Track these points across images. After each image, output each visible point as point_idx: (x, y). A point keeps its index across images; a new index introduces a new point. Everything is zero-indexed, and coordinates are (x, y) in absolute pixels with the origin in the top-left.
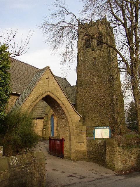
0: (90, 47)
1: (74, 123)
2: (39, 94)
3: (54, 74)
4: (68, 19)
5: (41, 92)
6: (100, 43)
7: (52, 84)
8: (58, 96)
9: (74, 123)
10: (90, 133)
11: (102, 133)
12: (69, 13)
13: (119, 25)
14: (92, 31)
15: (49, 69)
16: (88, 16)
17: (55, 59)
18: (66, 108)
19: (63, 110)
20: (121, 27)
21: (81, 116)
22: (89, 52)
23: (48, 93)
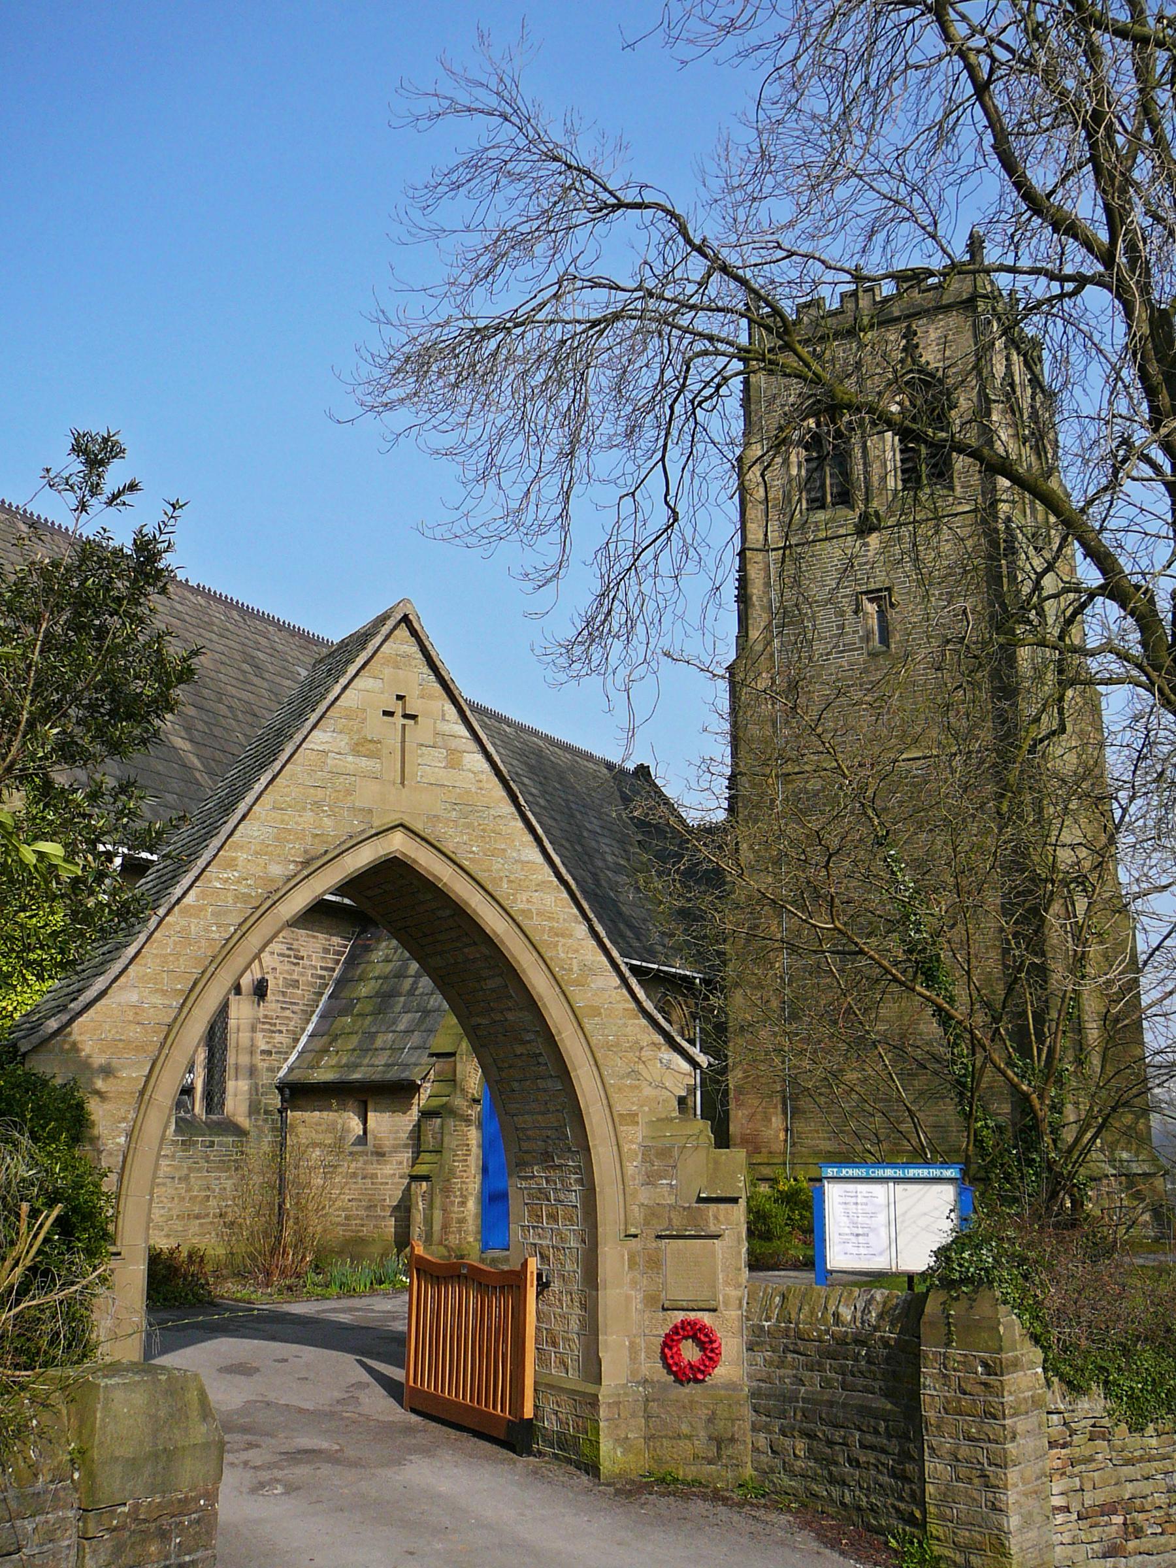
0: (844, 498)
1: (632, 1118)
2: (295, 850)
3: (467, 690)
4: (622, 251)
5: (332, 828)
6: (927, 461)
7: (429, 765)
8: (493, 869)
9: (632, 1118)
10: (785, 1231)
11: (888, 1221)
12: (620, 205)
13: (1082, 281)
14: (869, 369)
15: (414, 633)
16: (828, 253)
17: (516, 615)
18: (337, 699)
19: (531, 1005)
20: (1097, 298)
21: (703, 1060)
22: (838, 553)
23: (397, 843)
